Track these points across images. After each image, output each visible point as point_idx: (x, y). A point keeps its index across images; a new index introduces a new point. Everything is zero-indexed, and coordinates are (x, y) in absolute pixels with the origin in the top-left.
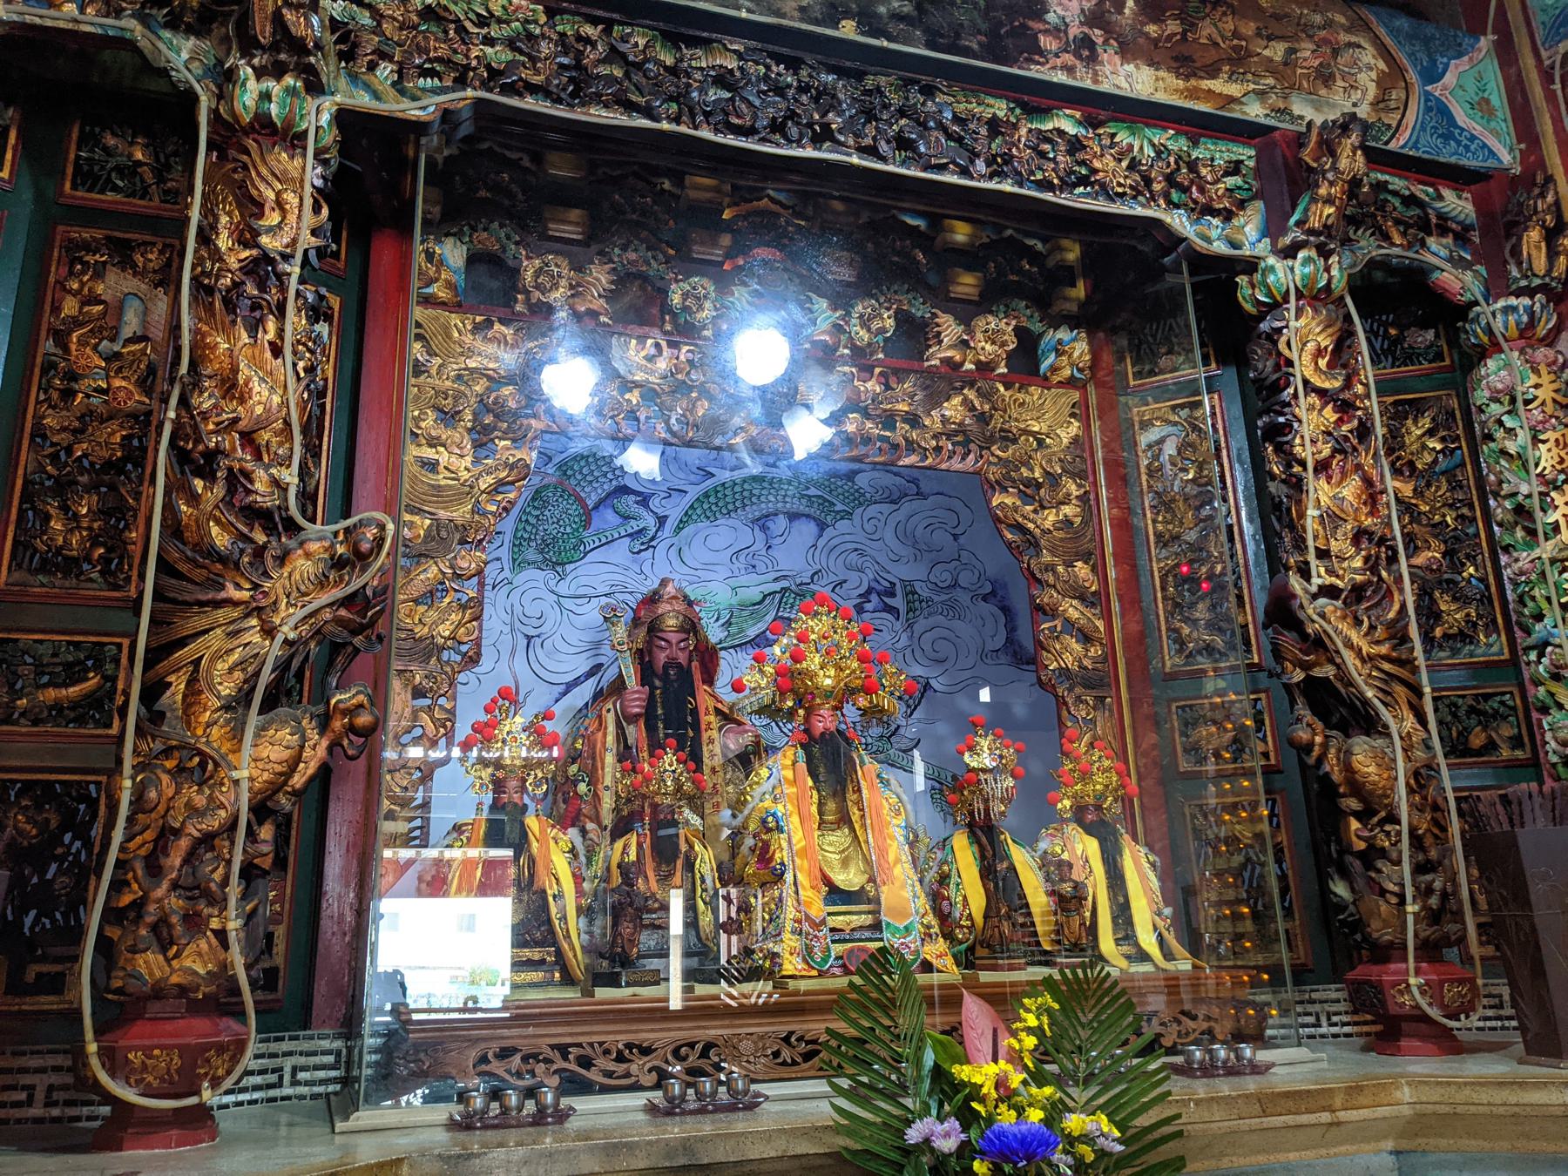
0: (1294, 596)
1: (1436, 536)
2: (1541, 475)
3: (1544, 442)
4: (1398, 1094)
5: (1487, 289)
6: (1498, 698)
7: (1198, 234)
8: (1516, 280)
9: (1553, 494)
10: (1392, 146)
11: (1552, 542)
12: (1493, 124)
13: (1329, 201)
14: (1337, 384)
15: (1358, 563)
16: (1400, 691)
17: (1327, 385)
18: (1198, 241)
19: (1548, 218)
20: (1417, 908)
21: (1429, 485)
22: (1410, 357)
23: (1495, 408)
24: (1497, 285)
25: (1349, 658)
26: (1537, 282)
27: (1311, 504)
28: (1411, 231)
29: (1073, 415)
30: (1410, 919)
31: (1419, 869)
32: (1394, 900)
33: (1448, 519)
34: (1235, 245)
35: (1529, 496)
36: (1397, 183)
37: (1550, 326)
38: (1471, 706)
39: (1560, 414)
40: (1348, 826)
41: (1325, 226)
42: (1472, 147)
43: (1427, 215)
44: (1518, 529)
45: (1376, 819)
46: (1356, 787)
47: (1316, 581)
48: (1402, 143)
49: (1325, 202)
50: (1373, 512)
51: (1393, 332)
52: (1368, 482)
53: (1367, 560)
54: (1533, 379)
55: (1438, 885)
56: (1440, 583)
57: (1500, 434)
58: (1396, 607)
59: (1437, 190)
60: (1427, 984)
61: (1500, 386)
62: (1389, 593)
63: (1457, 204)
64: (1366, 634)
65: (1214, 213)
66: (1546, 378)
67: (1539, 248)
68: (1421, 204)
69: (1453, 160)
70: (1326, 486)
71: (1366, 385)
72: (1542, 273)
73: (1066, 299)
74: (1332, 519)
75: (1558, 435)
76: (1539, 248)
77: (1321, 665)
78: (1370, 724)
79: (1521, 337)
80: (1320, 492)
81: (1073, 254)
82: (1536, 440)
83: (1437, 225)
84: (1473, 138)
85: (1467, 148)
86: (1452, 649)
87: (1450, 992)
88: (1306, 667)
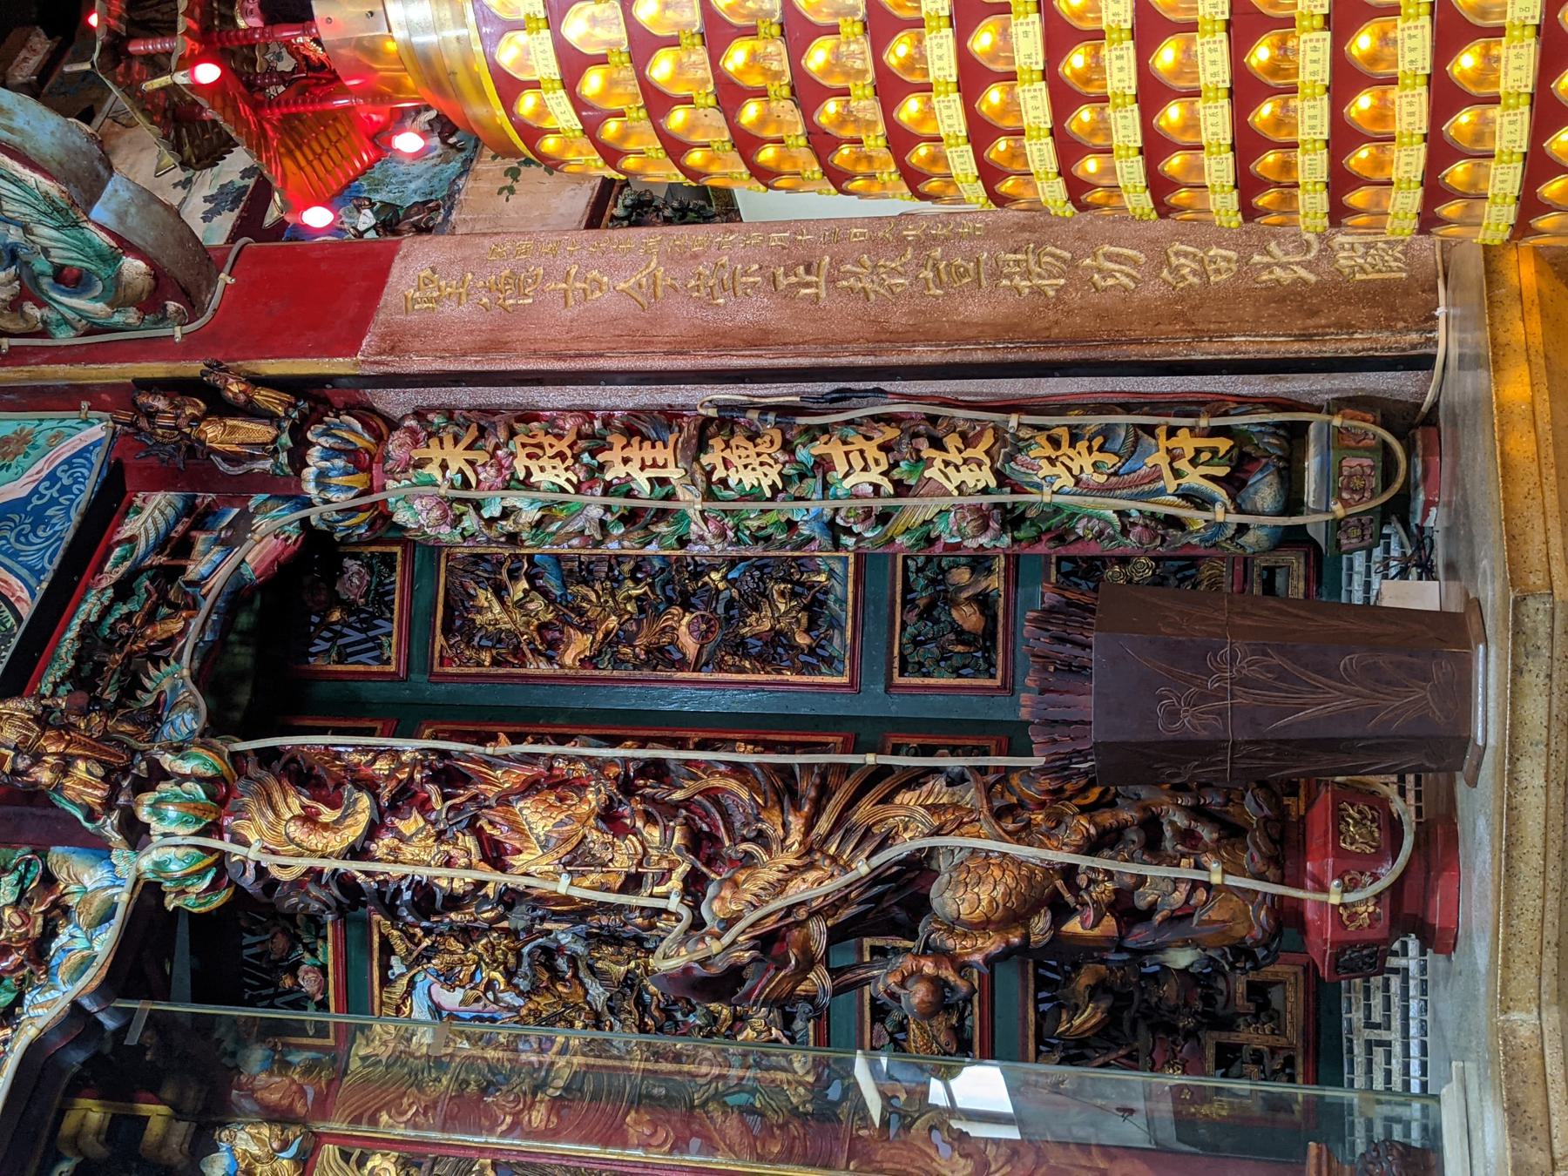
0: (687, 970)
1: (659, 616)
2: (578, 488)
3: (529, 474)
4: (1524, 1032)
5: (287, 498)
6: (912, 577)
7: (72, 981)
8: (277, 464)
9: (608, 477)
10: (26, 611)
11: (680, 492)
12: (41, 441)
13: (65, 766)
14: (365, 801)
15: (654, 834)
16: (865, 811)
17: (363, 819)
18: (85, 979)
19: (189, 411)
20: (1215, 866)
21: (581, 612)
22: (380, 598)
23: (470, 522)
24: (287, 491)
25: (799, 890)
26: (285, 439)
27: (549, 886)
28: (171, 595)
29: (361, 1163)
30: (1231, 881)
31: (1152, 847)
32: (1201, 895)
33: (634, 592)
34: (106, 916)
35: (607, 509)
36: (90, 608)
37: (358, 426)
38: (920, 617)
39: (492, 441)
40: (1075, 936)
41: (105, 779)
42: (66, 482)
43: (151, 567)
44: (653, 528)
45: (1068, 896)
46: (1015, 917)
47: (673, 904)
48: (25, 595)
49: (66, 774)
50: (580, 787)
51: (336, 616)
52: (530, 788)
53: (650, 819)
54: (433, 470)
55: (1181, 821)
56: (729, 619)
57: (508, 525)
58: (732, 784)
59: (119, 543)
60: (1341, 877)
61: (437, 513)
62: (712, 794)
63: (149, 516)
64: (768, 850)
65: (50, 933)
66: (434, 452)
67: (234, 429)
68: (134, 573)
69: (75, 517)
70: (524, 857)
71: (379, 753)
72: (274, 432)
73: (163, 1142)
74: (578, 859)
75: (522, 453)
76: (234, 429)
77: (808, 938)
78: (919, 867)
79: (368, 469)
80: (534, 869)
81: (92, 1113)
82: (526, 484)
83: (172, 555)
84: (52, 478)
85: (65, 490)
86: (831, 627)
87: (1357, 839)
88: (808, 963)
